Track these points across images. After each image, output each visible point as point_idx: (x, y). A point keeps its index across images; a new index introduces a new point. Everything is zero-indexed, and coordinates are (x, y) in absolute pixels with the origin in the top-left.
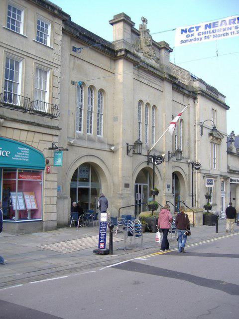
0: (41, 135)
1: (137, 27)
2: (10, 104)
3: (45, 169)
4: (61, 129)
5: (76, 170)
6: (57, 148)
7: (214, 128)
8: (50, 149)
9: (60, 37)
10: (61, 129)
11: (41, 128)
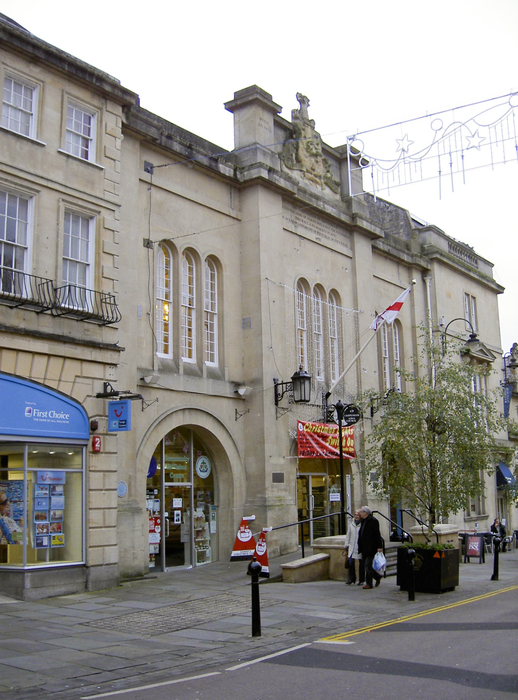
0: (77, 364)
1: (286, 115)
2: (9, 296)
3: (90, 443)
4: (123, 349)
5: (162, 441)
6: (116, 394)
7: (473, 337)
8: (99, 396)
9: (119, 142)
10: (123, 349)
11: (102, 351)
